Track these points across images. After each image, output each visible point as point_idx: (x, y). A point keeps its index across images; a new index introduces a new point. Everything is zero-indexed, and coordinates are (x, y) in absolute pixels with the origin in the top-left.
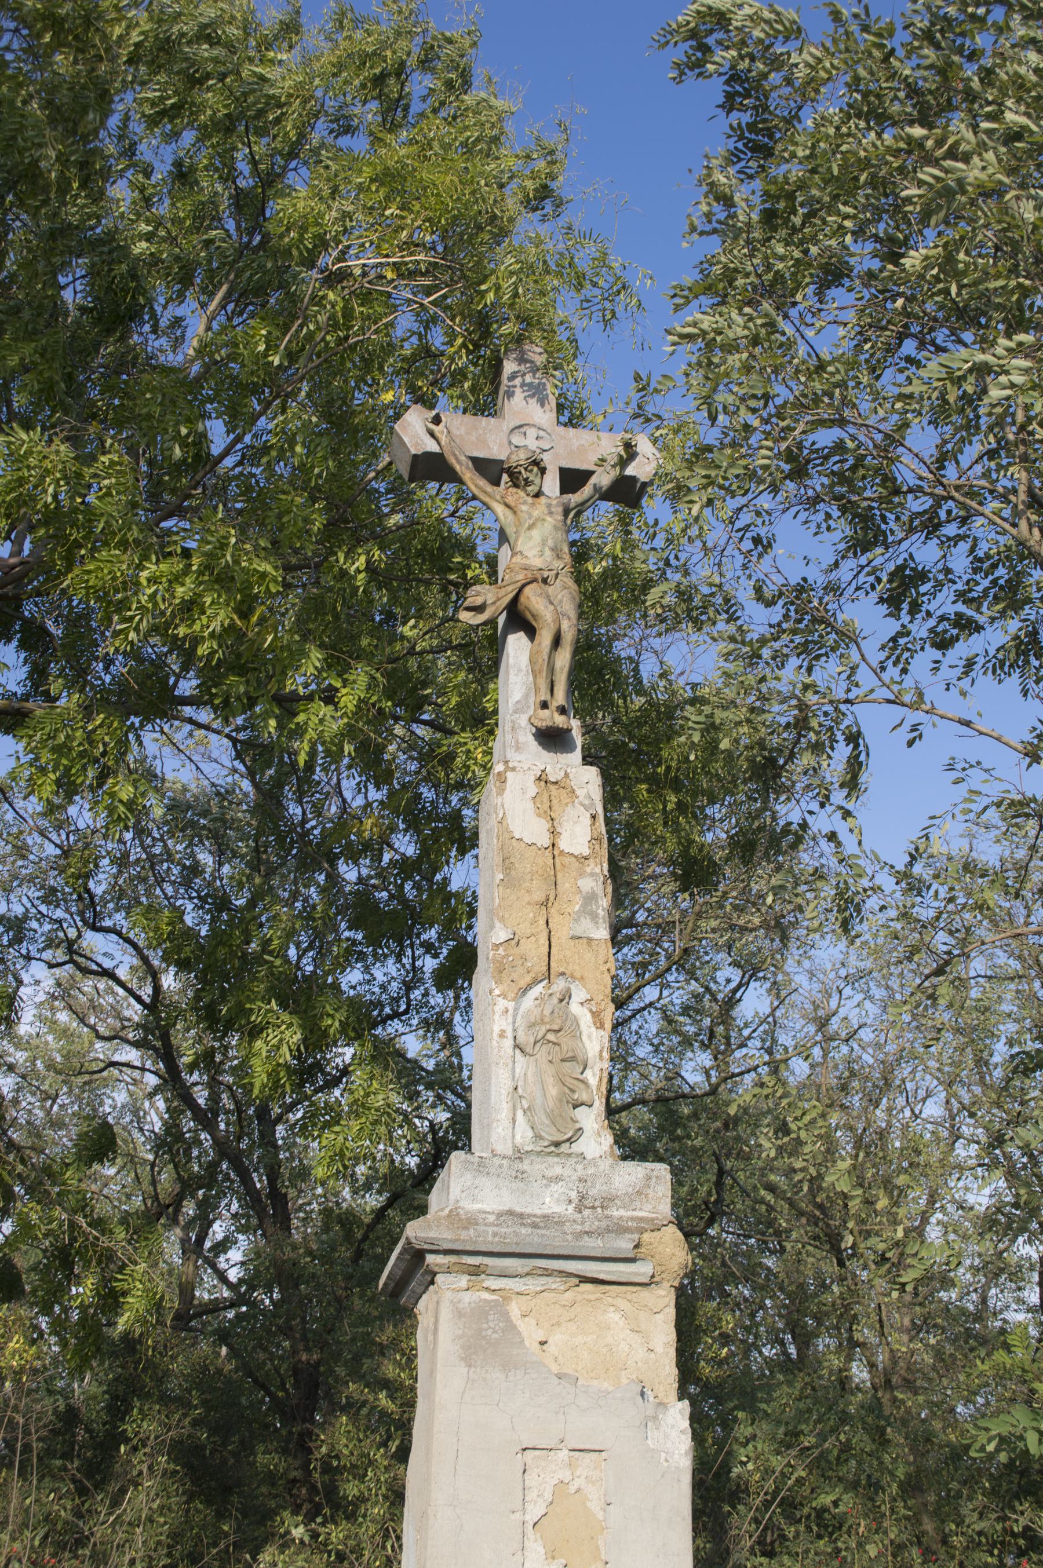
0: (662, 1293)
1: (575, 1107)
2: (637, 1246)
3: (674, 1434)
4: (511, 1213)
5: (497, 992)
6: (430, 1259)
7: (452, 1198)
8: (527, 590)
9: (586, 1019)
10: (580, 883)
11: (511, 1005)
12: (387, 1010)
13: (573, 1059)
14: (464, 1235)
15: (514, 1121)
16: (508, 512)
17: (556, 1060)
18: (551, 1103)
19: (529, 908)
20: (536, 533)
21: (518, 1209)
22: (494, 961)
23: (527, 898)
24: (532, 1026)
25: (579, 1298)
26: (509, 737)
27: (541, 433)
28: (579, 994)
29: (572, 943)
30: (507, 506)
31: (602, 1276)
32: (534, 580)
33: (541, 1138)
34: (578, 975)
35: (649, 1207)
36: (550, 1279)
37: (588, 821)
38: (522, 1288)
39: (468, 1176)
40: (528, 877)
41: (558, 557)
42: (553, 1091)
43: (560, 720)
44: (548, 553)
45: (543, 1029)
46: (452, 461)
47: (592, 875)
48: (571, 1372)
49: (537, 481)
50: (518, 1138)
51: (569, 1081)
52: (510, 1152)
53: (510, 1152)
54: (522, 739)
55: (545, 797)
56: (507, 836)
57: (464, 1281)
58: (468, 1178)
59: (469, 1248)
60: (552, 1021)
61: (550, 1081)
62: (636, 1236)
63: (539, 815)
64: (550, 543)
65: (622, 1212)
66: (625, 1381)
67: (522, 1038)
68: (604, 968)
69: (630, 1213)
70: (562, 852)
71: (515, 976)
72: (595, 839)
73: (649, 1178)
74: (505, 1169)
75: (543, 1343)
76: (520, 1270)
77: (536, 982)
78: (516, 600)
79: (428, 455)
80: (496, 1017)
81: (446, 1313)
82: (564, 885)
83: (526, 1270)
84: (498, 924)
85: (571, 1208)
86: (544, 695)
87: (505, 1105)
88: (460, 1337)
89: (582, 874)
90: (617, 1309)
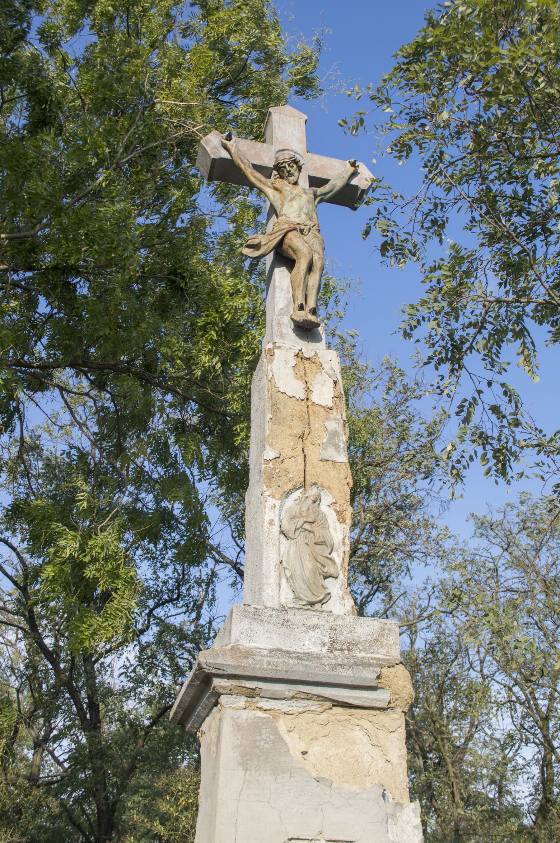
0: (396, 716)
1: (325, 578)
2: (378, 677)
3: (409, 829)
4: (279, 650)
5: (267, 493)
6: (216, 682)
7: (233, 637)
8: (290, 235)
9: (331, 516)
10: (326, 424)
11: (278, 503)
12: (166, 597)
13: (323, 543)
14: (244, 662)
15: (280, 586)
16: (276, 193)
17: (311, 543)
18: (308, 574)
20: (295, 204)
21: (284, 648)
22: (265, 471)
23: (289, 432)
24: (293, 518)
25: (332, 718)
26: (275, 329)
28: (327, 499)
29: (321, 464)
30: (276, 189)
31: (351, 701)
32: (295, 229)
33: (300, 599)
34: (326, 485)
35: (384, 651)
36: (310, 703)
37: (332, 385)
38: (287, 709)
39: (246, 621)
42: (309, 565)
45: (301, 521)
47: (335, 419)
48: (327, 776)
49: (296, 174)
51: (320, 559)
53: (277, 607)
54: (284, 331)
55: (301, 367)
57: (242, 701)
58: (246, 624)
59: (247, 674)
60: (308, 515)
62: (378, 669)
63: (297, 378)
64: (305, 210)
65: (363, 654)
66: (368, 785)
67: (286, 527)
68: (345, 482)
69: (369, 655)
71: (280, 483)
72: (336, 397)
73: (383, 630)
75: (304, 753)
76: (288, 694)
77: (295, 489)
78: (281, 242)
79: (223, 160)
80: (267, 510)
81: (227, 727)
82: (316, 426)
83: (292, 693)
84: (268, 447)
85: (325, 650)
86: (300, 300)
87: (273, 573)
89: (328, 419)
90: (362, 728)
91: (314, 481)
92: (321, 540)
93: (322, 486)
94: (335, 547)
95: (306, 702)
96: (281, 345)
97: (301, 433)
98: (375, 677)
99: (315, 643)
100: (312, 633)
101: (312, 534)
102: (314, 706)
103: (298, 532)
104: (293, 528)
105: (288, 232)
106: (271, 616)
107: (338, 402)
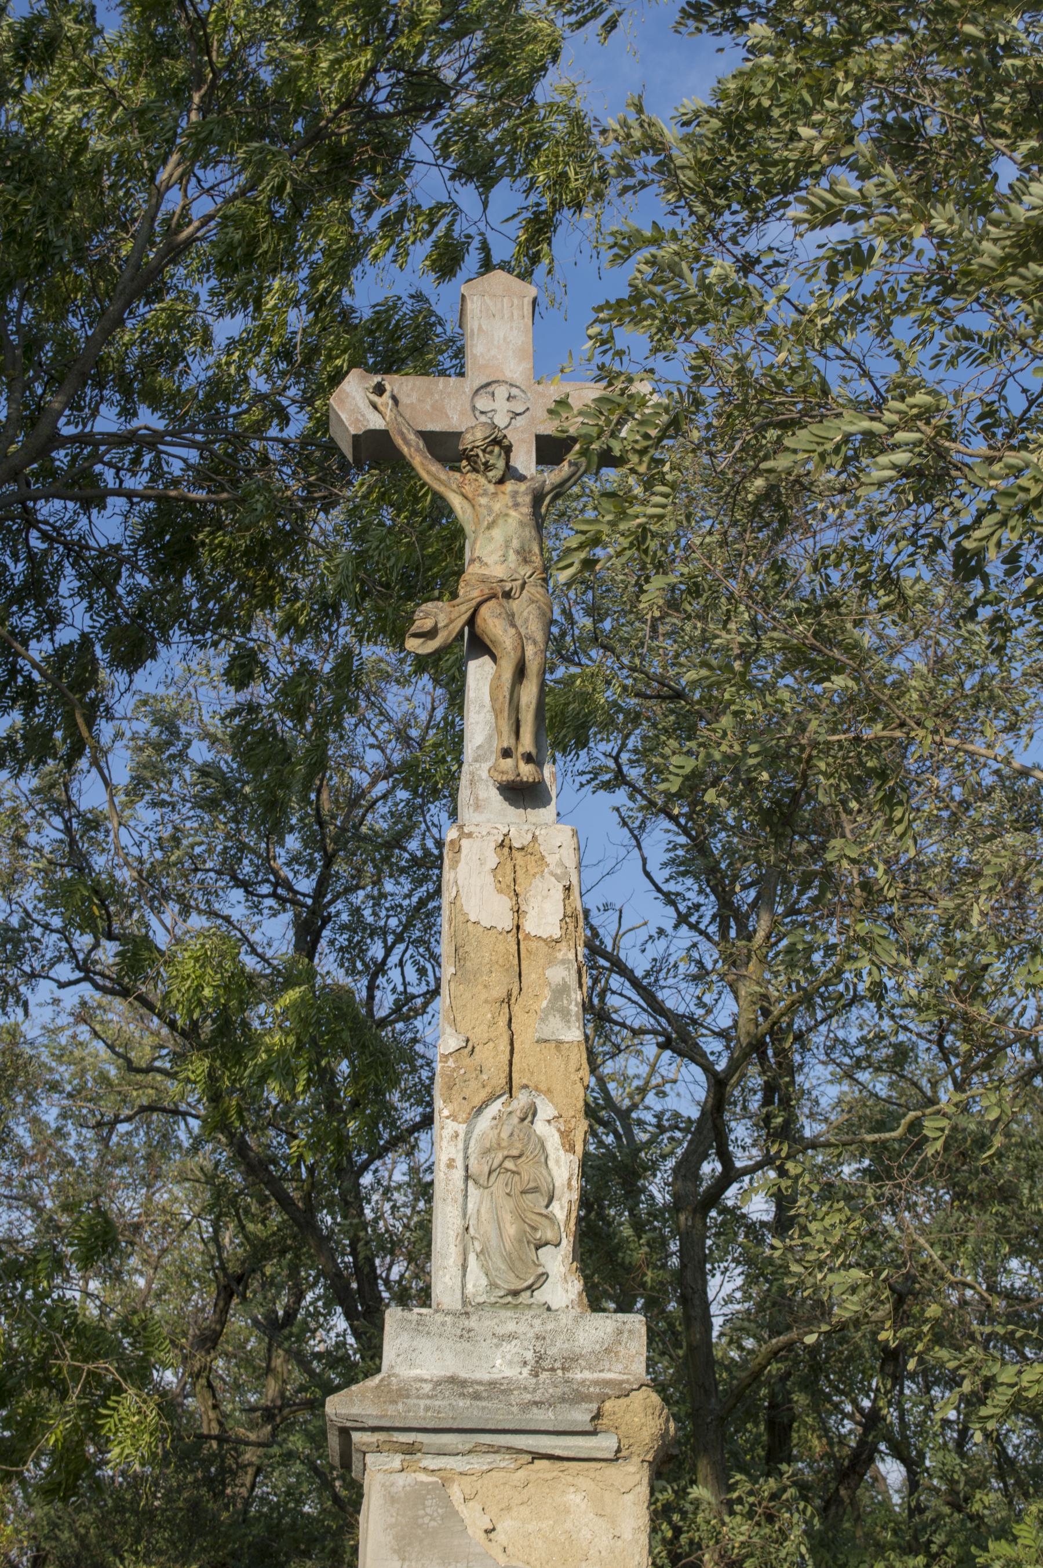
0: (632, 1469)
4: (452, 1380)
6: (356, 1437)
8: (484, 610)
11: (462, 1128)
13: (535, 1190)
14: (391, 1410)
15: (464, 1267)
19: (487, 1007)
20: (497, 533)
21: (463, 1375)
24: (486, 1152)
27: (514, 391)
28: (546, 1110)
31: (558, 1452)
34: (543, 1087)
35: (620, 1367)
37: (560, 895)
39: (405, 1336)
40: (485, 969)
41: (526, 561)
42: (511, 1230)
43: (527, 771)
44: (512, 557)
45: (500, 1156)
46: (399, 441)
47: (563, 962)
50: (470, 1287)
52: (458, 1306)
54: (482, 794)
56: (461, 918)
57: (397, 1461)
60: (511, 1145)
61: (507, 1217)
63: (500, 891)
64: (515, 544)
65: (587, 1375)
68: (575, 1077)
69: (596, 1376)
70: (528, 936)
71: (467, 1092)
73: (620, 1332)
74: (448, 1327)
75: (487, 1532)
77: (493, 1098)
78: (471, 621)
80: (444, 1144)
82: (530, 976)
83: (468, 1447)
85: (526, 1371)
86: (507, 742)
88: (392, 1526)
89: (551, 962)
91: (525, 1081)
92: (532, 1185)
93: (537, 1089)
94: (557, 1193)
95: (490, 1458)
96: (472, 829)
97: (505, 995)
98: (588, 1417)
99: (510, 1363)
100: (507, 1347)
101: (517, 1178)
102: (503, 1461)
103: (494, 1175)
104: (486, 1169)
105: (480, 604)
106: (443, 1324)
107: (571, 926)
